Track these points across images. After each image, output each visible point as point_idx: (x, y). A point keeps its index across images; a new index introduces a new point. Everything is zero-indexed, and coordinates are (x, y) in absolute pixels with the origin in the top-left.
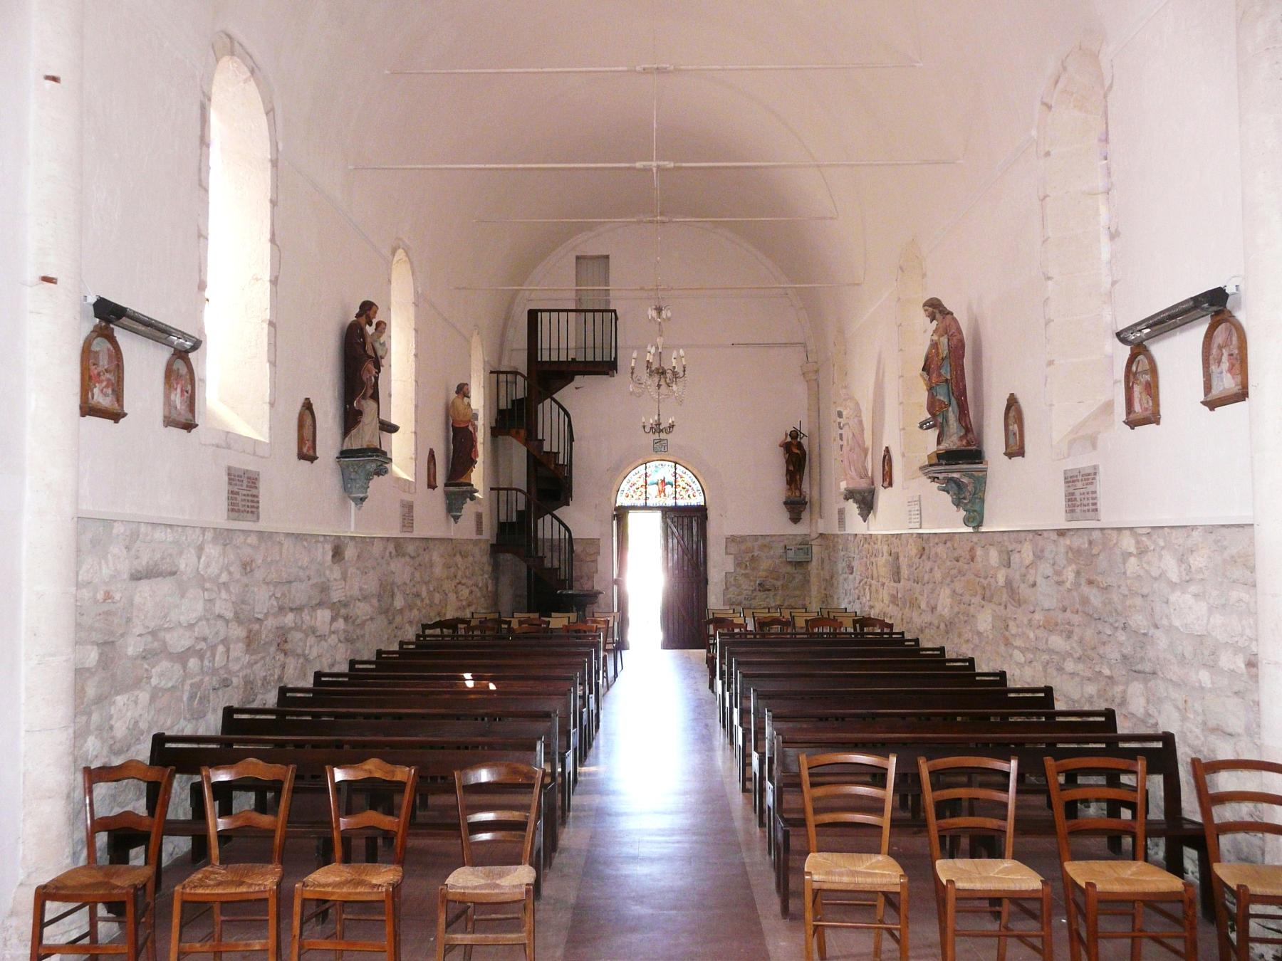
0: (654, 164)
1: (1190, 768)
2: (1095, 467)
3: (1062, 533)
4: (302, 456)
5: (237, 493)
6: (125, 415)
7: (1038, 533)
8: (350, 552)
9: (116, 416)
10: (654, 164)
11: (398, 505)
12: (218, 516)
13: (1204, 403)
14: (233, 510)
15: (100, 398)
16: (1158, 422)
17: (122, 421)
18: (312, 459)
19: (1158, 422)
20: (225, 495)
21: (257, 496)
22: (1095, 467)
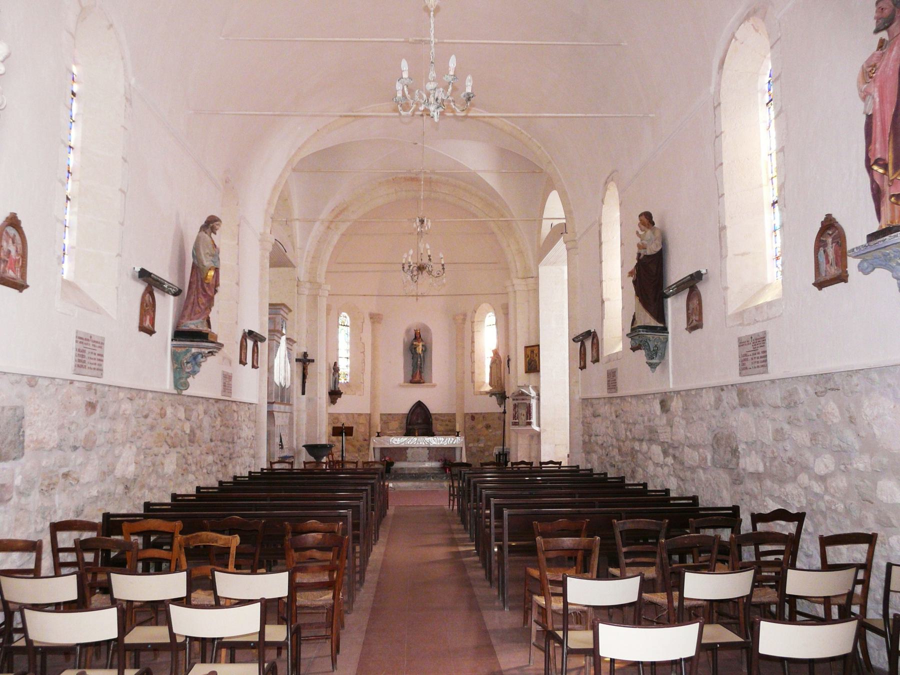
0: (432, 39)
1: (403, 445)
2: (765, 333)
3: (217, 401)
4: (142, 329)
5: (84, 351)
6: (27, 286)
7: (207, 399)
8: (676, 405)
9: (20, 286)
10: (432, 39)
11: (73, 339)
12: (65, 368)
13: (814, 284)
14: (79, 361)
15: (147, 324)
16: (846, 281)
17: (25, 291)
18: (151, 332)
19: (846, 281)
20: (73, 353)
21: (102, 356)
22: (765, 333)
